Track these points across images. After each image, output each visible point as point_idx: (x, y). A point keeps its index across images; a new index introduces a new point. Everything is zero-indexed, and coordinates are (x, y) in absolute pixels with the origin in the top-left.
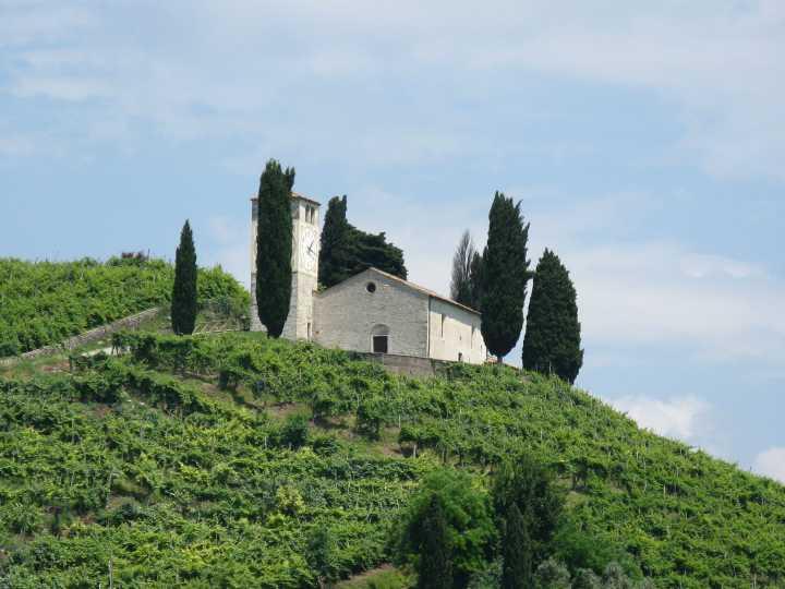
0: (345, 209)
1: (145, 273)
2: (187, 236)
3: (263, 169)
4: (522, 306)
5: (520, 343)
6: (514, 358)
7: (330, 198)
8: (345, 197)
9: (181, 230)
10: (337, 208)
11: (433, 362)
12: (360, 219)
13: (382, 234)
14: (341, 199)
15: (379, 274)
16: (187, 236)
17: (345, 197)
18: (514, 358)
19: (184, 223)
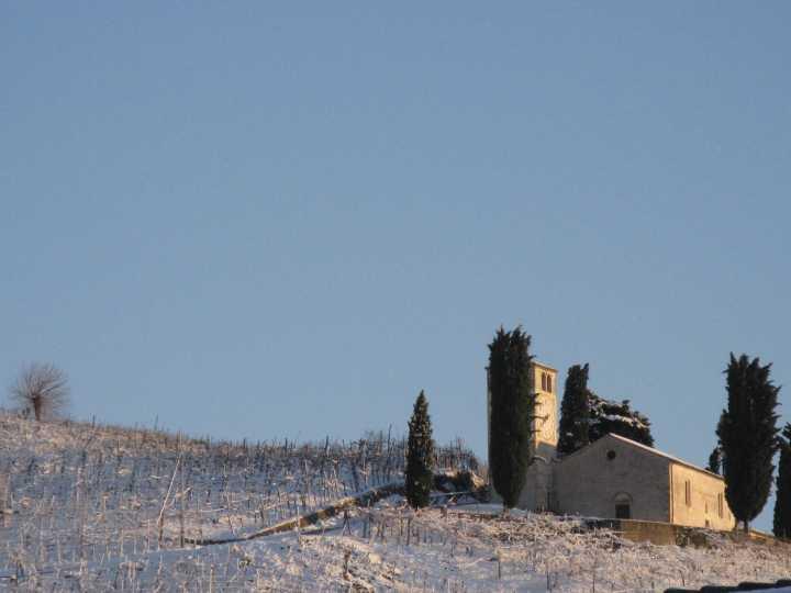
0: (587, 378)
1: (365, 455)
2: (420, 406)
3: (484, 358)
4: (777, 492)
5: (772, 500)
6: (764, 522)
7: (571, 365)
8: (587, 365)
9: (415, 402)
10: (577, 377)
11: (675, 528)
12: (603, 388)
13: (626, 402)
14: (582, 368)
15: (599, 516)
16: (420, 406)
17: (587, 365)
18: (764, 522)
19: (418, 395)
